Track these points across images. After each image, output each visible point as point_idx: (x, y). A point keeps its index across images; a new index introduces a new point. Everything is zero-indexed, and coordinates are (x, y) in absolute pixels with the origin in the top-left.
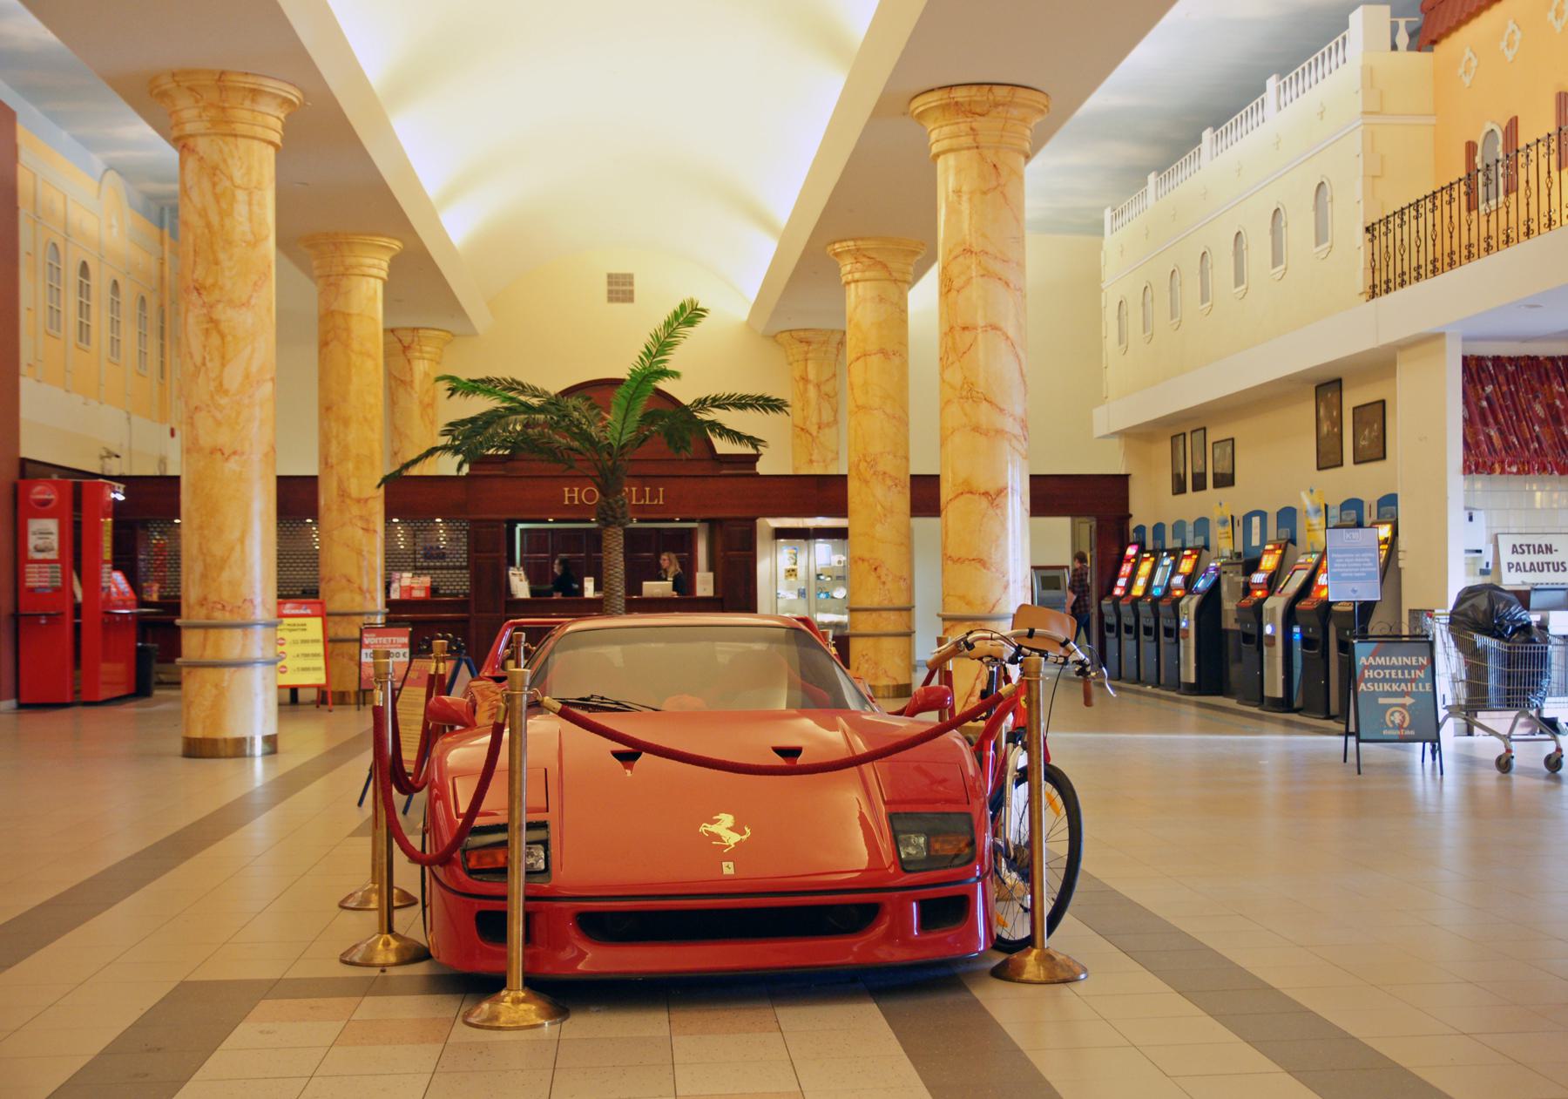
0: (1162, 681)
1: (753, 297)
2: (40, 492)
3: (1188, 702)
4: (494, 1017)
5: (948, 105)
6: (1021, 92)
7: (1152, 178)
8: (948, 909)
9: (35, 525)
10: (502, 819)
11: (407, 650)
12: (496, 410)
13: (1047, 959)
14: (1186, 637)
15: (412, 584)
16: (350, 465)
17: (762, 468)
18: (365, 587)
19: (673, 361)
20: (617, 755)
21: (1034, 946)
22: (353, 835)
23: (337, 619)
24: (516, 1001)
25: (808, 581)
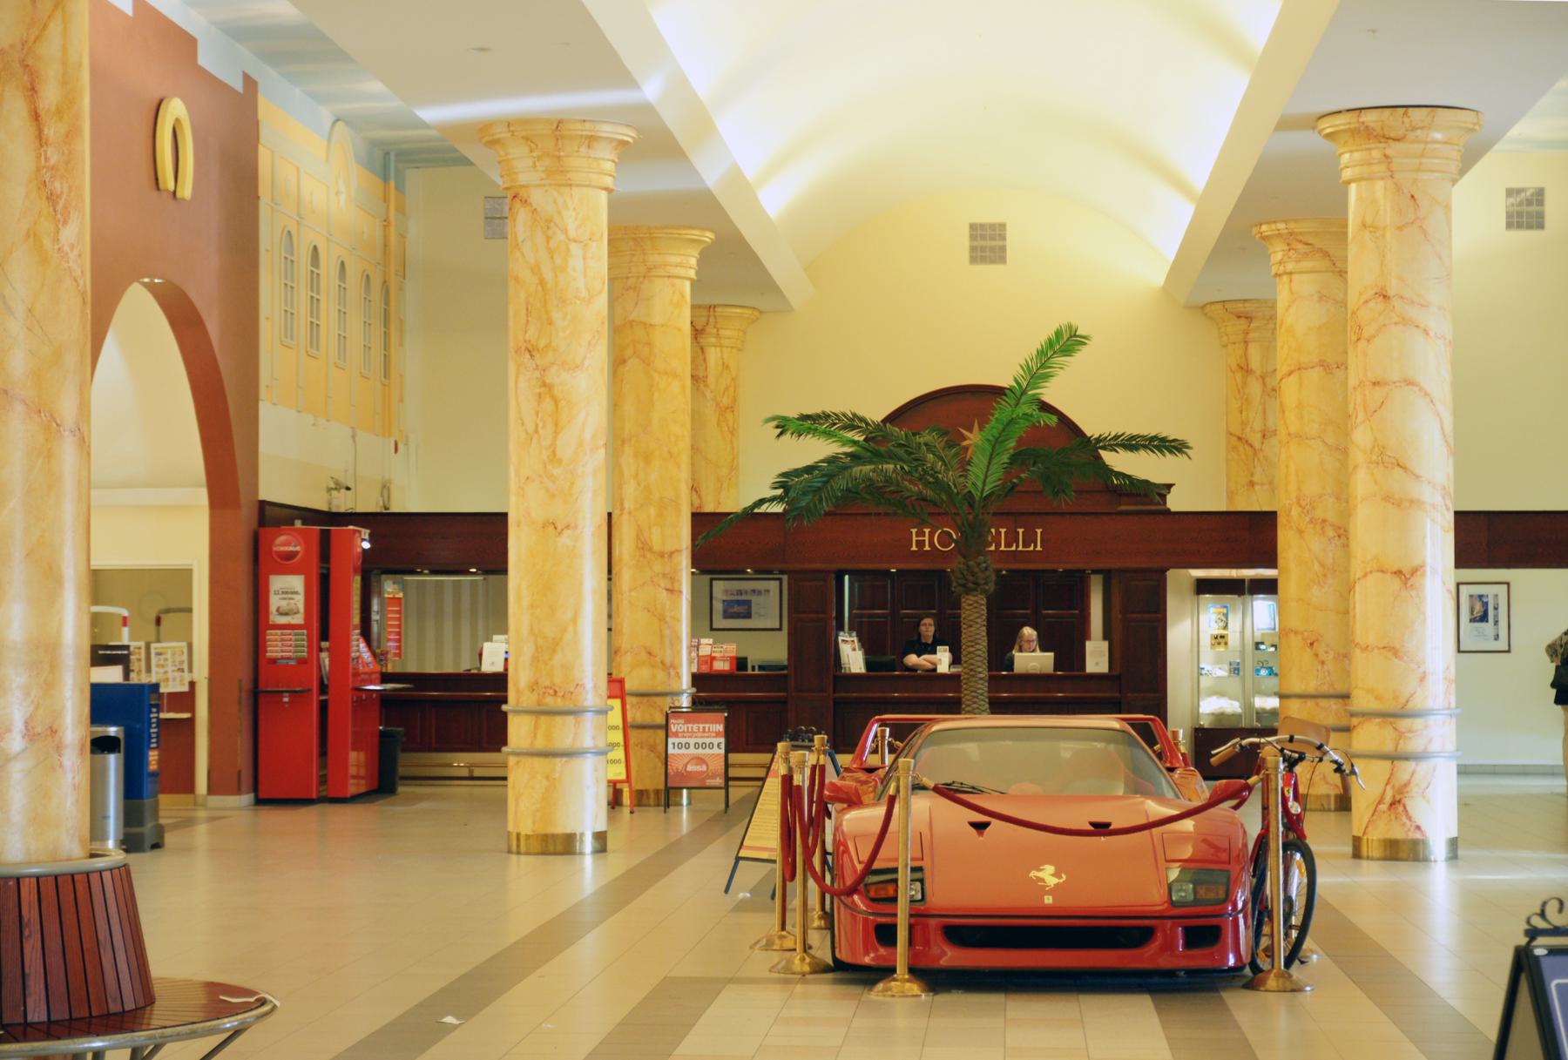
2: (285, 542)
8: (1204, 933)
9: (278, 583)
11: (722, 740)
12: (832, 460)
15: (721, 653)
16: (652, 511)
17: (1175, 503)
18: (668, 661)
20: (973, 825)
25: (1243, 652)
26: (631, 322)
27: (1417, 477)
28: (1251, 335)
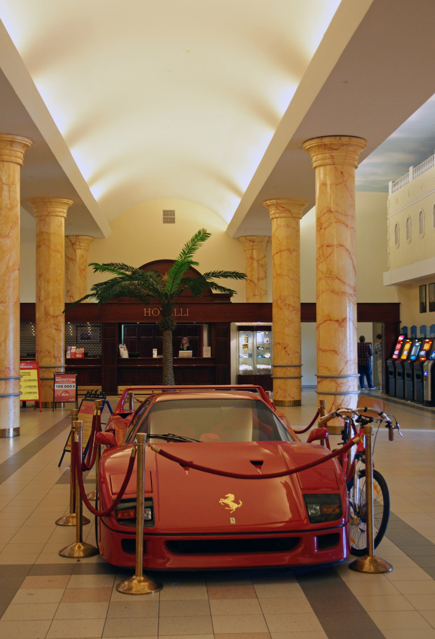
0: (415, 398)
1: (229, 221)
3: (427, 411)
4: (130, 589)
5: (321, 145)
6: (353, 138)
7: (411, 169)
8: (331, 540)
10: (134, 496)
11: (75, 384)
12: (114, 280)
13: (374, 561)
14: (427, 380)
15: (77, 351)
16: (50, 301)
17: (233, 300)
18: (56, 355)
19: (195, 257)
21: (368, 555)
22: (57, 483)
23: (44, 369)
24: (140, 581)
25: (253, 350)
26: (42, 232)
27: (344, 283)
28: (254, 247)
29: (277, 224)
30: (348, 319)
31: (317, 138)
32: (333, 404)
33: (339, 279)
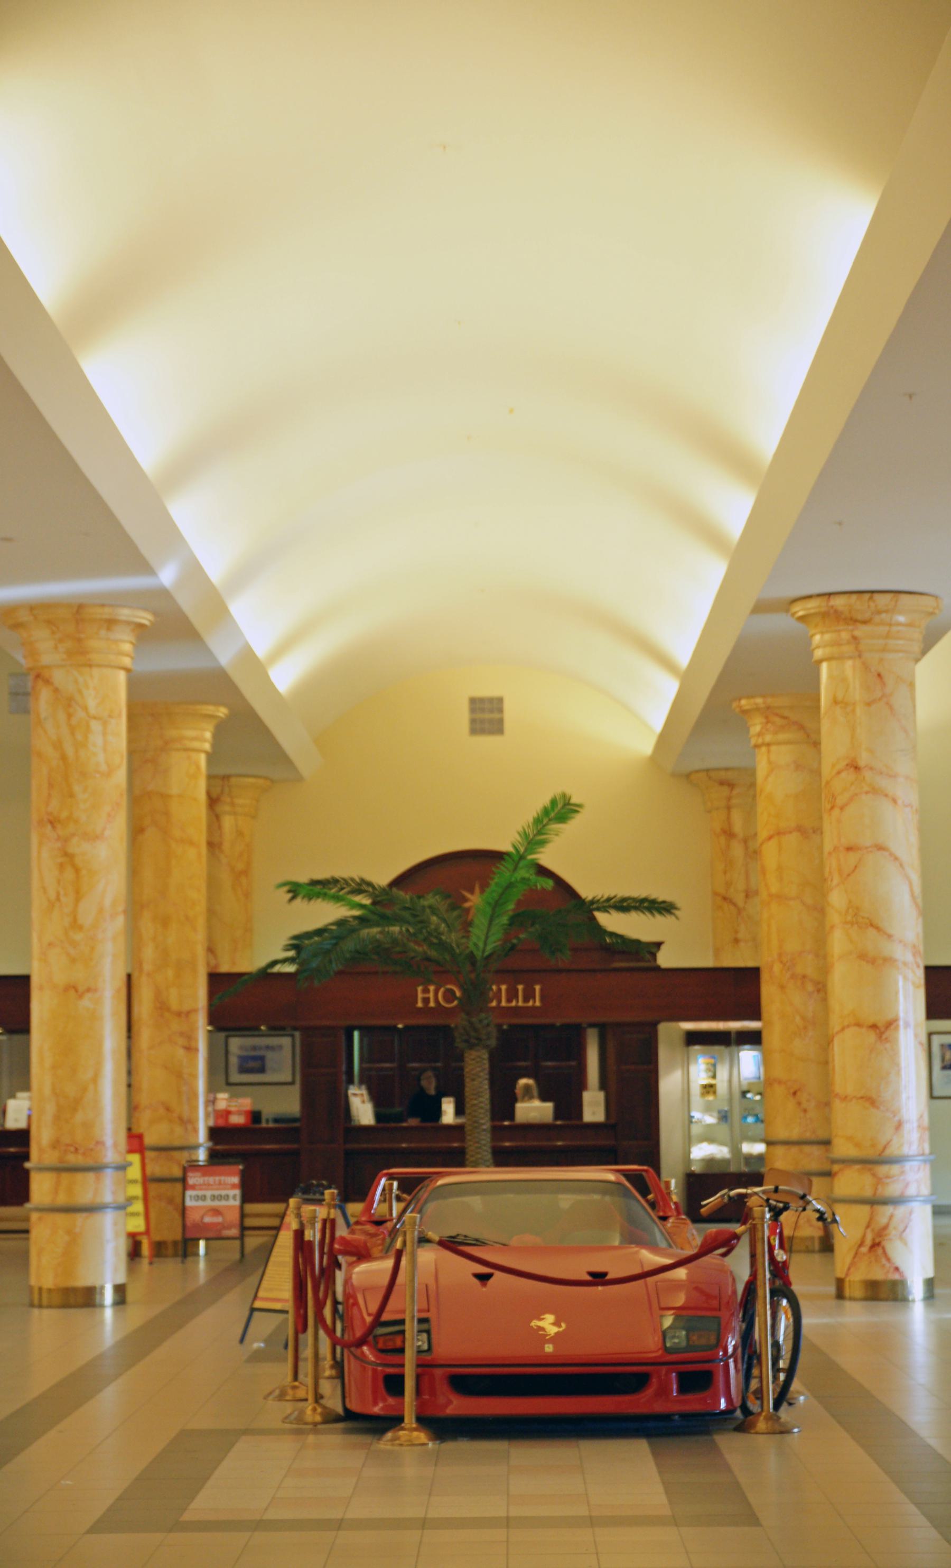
11: (237, 1192)
12: (341, 923)
15: (236, 1107)
16: (170, 973)
17: (665, 960)
27: (890, 936)
29: (770, 762)
30: (901, 1023)
31: (819, 595)
32: (868, 1227)
33: (878, 929)
